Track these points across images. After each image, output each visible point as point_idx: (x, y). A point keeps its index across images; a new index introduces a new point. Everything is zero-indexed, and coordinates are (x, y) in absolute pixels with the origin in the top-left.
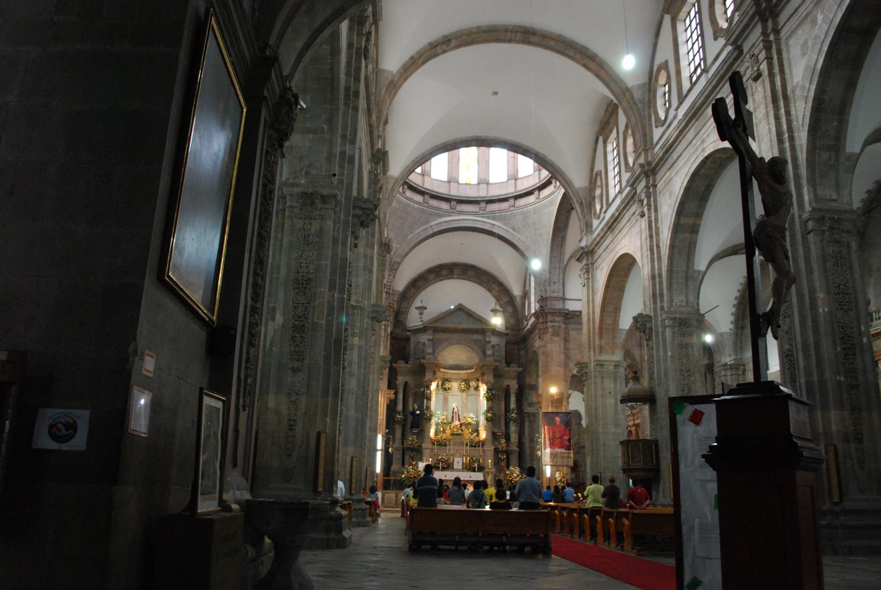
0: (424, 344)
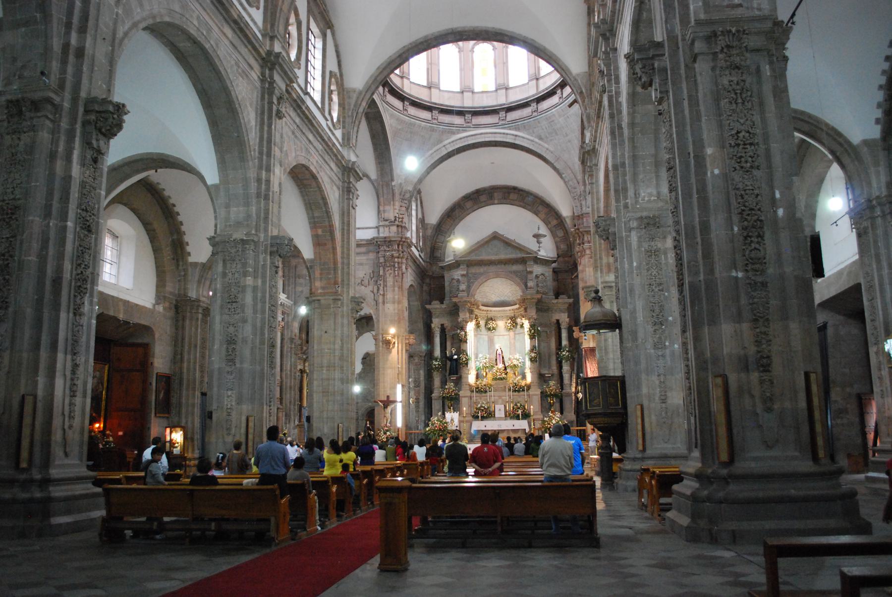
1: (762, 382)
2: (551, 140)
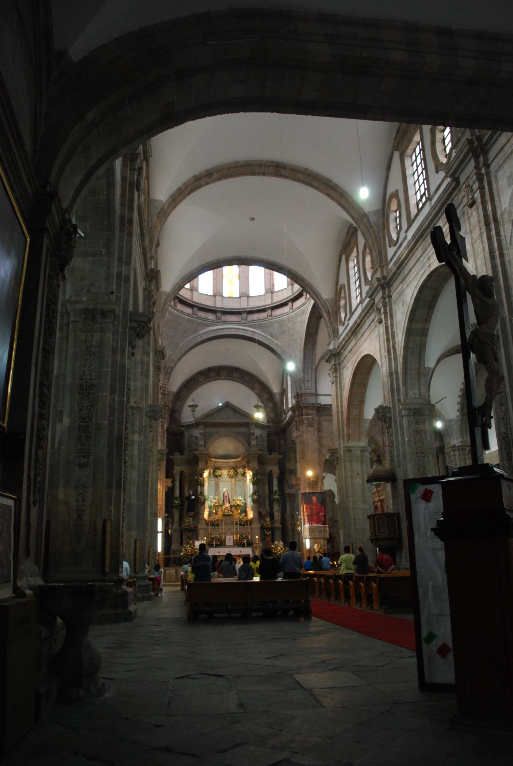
0: (197, 438)
2: (280, 338)
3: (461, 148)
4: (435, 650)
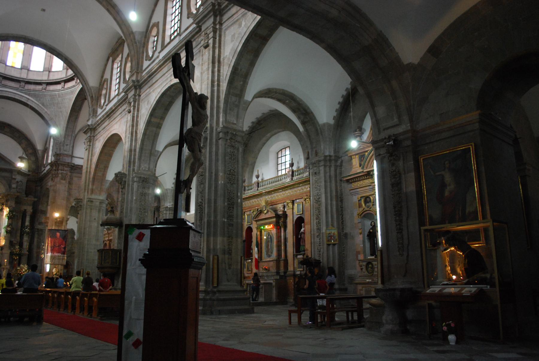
1: (228, 259)
3: (206, 7)
4: (131, 343)
